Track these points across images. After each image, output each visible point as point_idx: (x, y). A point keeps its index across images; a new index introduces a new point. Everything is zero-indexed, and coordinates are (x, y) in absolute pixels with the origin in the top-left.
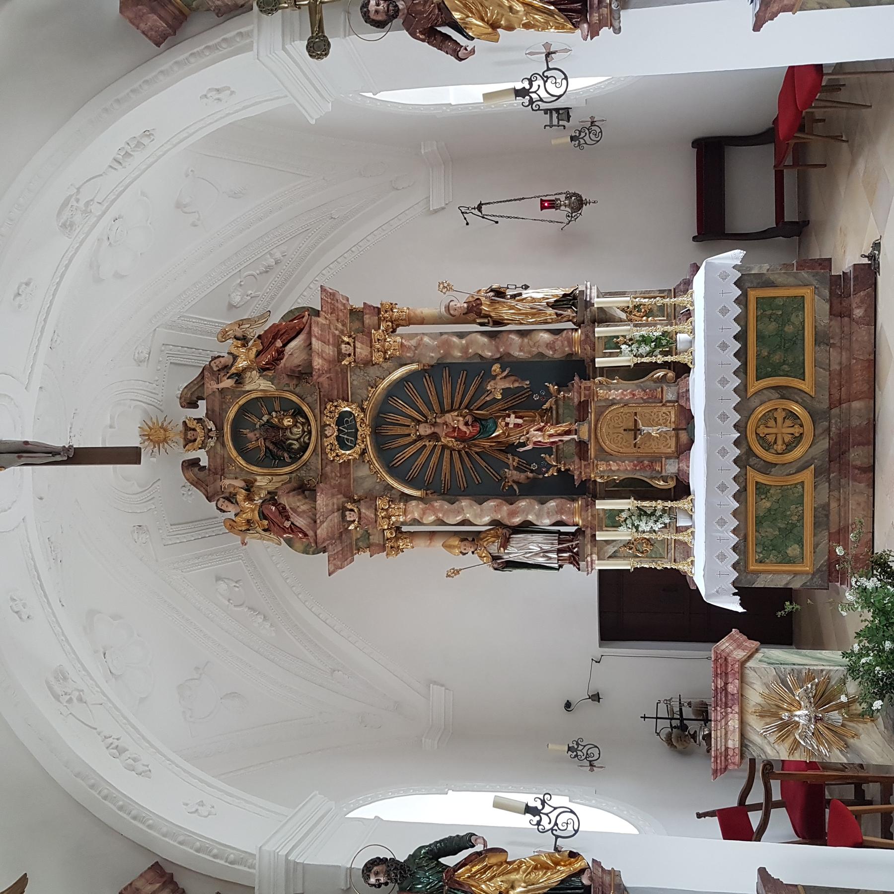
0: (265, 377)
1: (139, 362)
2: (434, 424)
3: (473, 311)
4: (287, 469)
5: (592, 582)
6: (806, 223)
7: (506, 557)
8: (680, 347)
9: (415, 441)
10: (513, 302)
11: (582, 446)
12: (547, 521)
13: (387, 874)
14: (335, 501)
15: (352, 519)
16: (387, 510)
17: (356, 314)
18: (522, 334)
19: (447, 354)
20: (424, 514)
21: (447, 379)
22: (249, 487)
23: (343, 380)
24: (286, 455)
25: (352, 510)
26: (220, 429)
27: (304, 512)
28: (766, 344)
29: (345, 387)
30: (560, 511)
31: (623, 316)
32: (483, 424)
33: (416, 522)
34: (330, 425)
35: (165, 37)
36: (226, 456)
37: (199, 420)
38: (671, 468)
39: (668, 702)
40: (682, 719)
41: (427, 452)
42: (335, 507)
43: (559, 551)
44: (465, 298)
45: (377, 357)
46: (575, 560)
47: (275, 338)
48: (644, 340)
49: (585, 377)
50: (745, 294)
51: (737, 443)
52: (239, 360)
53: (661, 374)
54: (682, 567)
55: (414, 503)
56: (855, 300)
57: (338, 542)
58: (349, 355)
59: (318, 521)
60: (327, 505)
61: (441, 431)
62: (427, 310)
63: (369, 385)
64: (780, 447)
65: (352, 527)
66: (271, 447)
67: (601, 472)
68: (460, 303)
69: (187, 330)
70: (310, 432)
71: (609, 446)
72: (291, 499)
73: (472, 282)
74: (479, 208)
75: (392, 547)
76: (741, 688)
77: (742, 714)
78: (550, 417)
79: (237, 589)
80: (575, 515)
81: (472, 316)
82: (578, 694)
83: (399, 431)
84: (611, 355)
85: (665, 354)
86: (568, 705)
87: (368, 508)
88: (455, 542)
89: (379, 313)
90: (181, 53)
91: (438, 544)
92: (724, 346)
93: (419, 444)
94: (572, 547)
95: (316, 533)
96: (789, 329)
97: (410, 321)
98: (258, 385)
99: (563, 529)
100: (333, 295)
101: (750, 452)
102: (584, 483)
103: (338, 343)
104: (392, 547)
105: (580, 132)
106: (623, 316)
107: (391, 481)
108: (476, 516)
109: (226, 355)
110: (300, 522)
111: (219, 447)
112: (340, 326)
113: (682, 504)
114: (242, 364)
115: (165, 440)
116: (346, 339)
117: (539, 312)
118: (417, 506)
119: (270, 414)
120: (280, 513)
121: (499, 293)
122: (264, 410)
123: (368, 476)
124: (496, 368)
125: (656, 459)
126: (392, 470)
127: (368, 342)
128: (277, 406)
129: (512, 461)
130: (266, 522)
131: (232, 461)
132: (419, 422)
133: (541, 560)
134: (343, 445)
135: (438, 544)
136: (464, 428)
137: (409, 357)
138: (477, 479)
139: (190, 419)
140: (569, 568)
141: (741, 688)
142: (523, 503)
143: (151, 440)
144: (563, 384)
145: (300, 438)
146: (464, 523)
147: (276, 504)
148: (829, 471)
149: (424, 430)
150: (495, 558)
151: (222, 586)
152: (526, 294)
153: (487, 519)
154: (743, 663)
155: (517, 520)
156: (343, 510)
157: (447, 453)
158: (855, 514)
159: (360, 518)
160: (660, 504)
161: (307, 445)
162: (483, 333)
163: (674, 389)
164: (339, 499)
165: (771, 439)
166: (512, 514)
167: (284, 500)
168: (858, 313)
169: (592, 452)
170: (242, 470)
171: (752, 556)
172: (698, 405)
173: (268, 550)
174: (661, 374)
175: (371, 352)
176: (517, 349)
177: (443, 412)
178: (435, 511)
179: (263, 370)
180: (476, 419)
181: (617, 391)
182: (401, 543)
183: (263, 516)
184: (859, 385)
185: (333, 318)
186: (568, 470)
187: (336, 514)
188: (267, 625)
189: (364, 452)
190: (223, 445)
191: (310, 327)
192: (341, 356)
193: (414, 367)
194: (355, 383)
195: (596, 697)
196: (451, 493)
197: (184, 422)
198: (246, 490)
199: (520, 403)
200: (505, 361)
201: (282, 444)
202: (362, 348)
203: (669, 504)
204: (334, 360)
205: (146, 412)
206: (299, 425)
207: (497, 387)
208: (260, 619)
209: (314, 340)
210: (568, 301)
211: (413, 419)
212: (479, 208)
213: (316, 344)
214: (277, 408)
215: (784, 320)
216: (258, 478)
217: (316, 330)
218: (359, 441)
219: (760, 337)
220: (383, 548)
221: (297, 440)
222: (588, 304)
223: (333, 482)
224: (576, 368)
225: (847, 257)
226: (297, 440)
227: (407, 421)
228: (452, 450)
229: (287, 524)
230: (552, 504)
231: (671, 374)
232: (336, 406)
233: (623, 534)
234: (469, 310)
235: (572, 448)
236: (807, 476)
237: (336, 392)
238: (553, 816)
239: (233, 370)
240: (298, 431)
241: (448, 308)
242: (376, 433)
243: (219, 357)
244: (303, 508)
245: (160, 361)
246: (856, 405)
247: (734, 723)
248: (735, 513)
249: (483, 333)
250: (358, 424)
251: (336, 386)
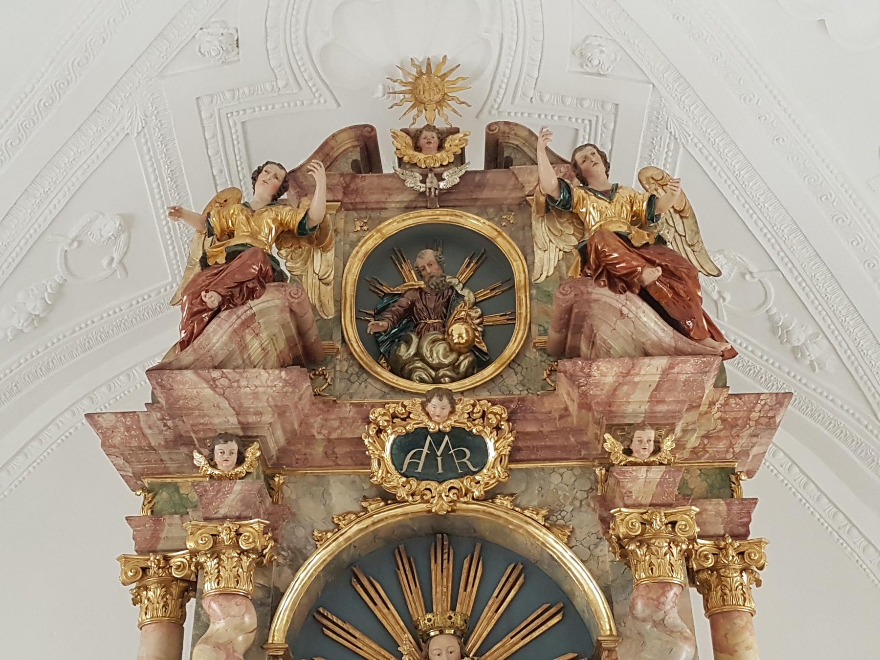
1: (582, 55)
4: (352, 334)
9: (412, 627)
14: (268, 418)
15: (218, 458)
16: (236, 546)
17: (724, 482)
20: (217, 646)
23: (564, 448)
24: (384, 324)
25: (240, 460)
26: (444, 199)
27: (244, 347)
29: (543, 454)
33: (203, 624)
34: (453, 412)
36: (384, 214)
37: (460, 159)
42: (252, 419)
52: (604, 204)
55: (250, 620)
57: (169, 434)
58: (628, 452)
59: (216, 374)
60: (256, 395)
63: (551, 512)
65: (199, 459)
66: (404, 302)
72: (276, 316)
75: (144, 569)
79: (105, 262)
83: (440, 590)
87: (245, 502)
89: (735, 537)
95: (186, 368)
97: (720, 618)
100: (771, 425)
103: (663, 425)
104: (144, 569)
107: (316, 560)
109: (612, 181)
111: (406, 198)
112: (693, 441)
114: (593, 211)
115: (419, 103)
116: (668, 444)
118: (240, 629)
119: (476, 304)
120: (241, 284)
122: (484, 294)
123: (329, 510)
126: (343, 573)
127: (664, 499)
130: (221, 260)
131: (374, 224)
132: (463, 636)
134: (409, 443)
137: (632, 607)
139: (464, 140)
143: (417, 78)
145: (423, 360)
151: (110, 226)
159: (220, 478)
167: (269, 302)
170: (353, 245)
175: (640, 506)
182: (154, 593)
185: (713, 423)
187: (233, 420)
189: (388, 498)
190: (409, 208)
191: (693, 354)
192: (625, 432)
193: (606, 625)
194: (556, 479)
197: (457, 131)
198: (302, 224)
201: (409, 321)
202: (647, 482)
204: (610, 414)
206: (453, 356)
209: (662, 362)
211: (471, 623)
213: (652, 369)
214: (489, 320)
216: (330, 255)
217: (687, 367)
218: (414, 482)
221: (418, 354)
223: (316, 422)
226: (418, 354)
227: (465, 605)
229: (212, 299)
232: (498, 428)
237: (531, 428)
239: (578, 193)
240: (438, 354)
243: (607, 166)
244: (254, 347)
245: (580, 101)
250: (455, 483)
251: (546, 429)
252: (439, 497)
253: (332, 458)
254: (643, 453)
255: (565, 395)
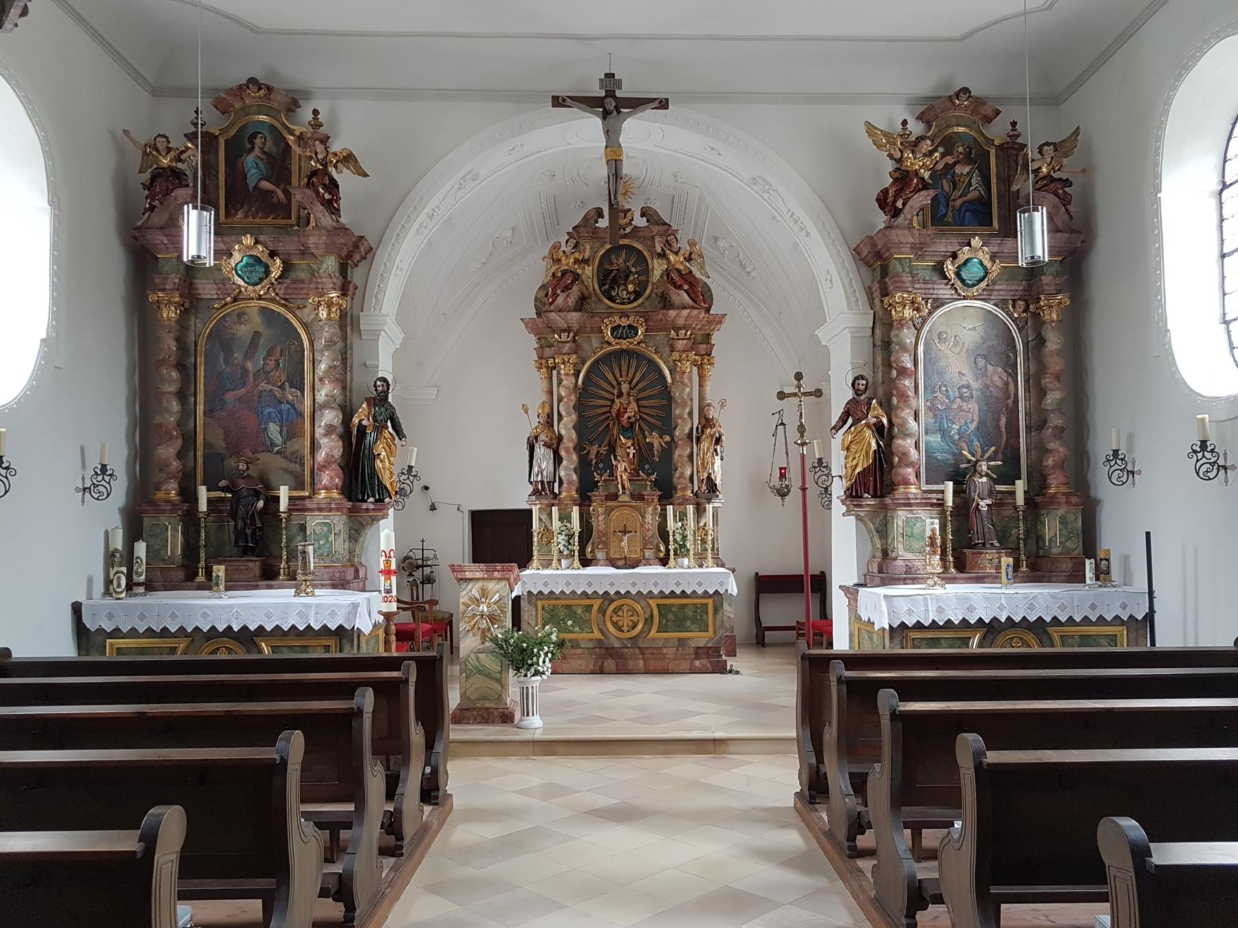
0: (661, 276)
2: (629, 395)
3: (707, 422)
5: (523, 505)
6: (764, 645)
7: (537, 446)
8: (679, 560)
10: (712, 450)
11: (615, 497)
12: (562, 474)
13: (383, 391)
18: (691, 456)
19: (678, 405)
21: (660, 404)
22: (585, 261)
28: (679, 611)
30: (569, 483)
31: (702, 524)
32: (628, 430)
35: (859, 254)
38: (600, 555)
39: (435, 557)
40: (423, 566)
41: (611, 389)
43: (542, 482)
44: (716, 416)
45: (676, 355)
46: (536, 492)
47: (690, 283)
48: (684, 538)
49: (660, 498)
50: (710, 596)
51: (618, 593)
53: (662, 549)
54: (535, 563)
55: (574, 381)
56: (705, 662)
61: (624, 400)
62: (708, 389)
64: (615, 619)
67: (598, 509)
68: (712, 414)
69: (696, 224)
70: (623, 303)
71: (615, 514)
73: (727, 422)
74: (782, 424)
76: (496, 579)
77: (483, 579)
78: (634, 476)
80: (569, 492)
81: (703, 422)
82: (435, 495)
83: (624, 368)
84: (675, 516)
85: (675, 551)
86: (426, 488)
88: (547, 411)
90: (849, 263)
91: (544, 397)
92: (678, 584)
93: (614, 383)
94: (543, 490)
96: (688, 623)
97: (702, 377)
98: (658, 268)
99: (556, 485)
101: (612, 601)
102: (589, 498)
103: (686, 328)
105: (1122, 459)
106: (702, 524)
107: (588, 364)
108: (565, 425)
110: (560, 300)
113: (577, 563)
114: (672, 257)
117: (704, 468)
121: (718, 441)
122: (639, 268)
124: (668, 438)
125: (606, 545)
126: (596, 362)
128: (641, 278)
129: (603, 450)
133: (535, 469)
134: (613, 329)
135: (544, 397)
136: (626, 416)
138: (590, 424)
140: (531, 489)
141: (496, 579)
142: (575, 457)
144: (656, 484)
146: (559, 414)
147: (573, 282)
148: (600, 648)
149: (625, 388)
150: (536, 438)
151: (509, 233)
152: (717, 459)
153: (563, 432)
154: (508, 579)
155: (563, 453)
156: (568, 330)
157: (609, 403)
158: (575, 664)
160: (576, 548)
161: (614, 301)
162: (692, 429)
163: (652, 556)
164: (575, 327)
165: (620, 613)
166: (567, 450)
168: (697, 663)
169: (610, 503)
171: (546, 603)
172: (641, 570)
173: (537, 272)
174: (662, 549)
176: (680, 453)
177: (637, 401)
178: (568, 396)
179: (667, 273)
180: (632, 424)
181: (651, 520)
183: (564, 273)
184: (652, 665)
186: (597, 487)
188: (479, 266)
192: (677, 329)
193: (669, 380)
195: (433, 508)
196: (580, 407)
199: (644, 453)
200: (672, 445)
201: (615, 283)
203: (577, 554)
205: (638, 178)
207: (655, 439)
208: (484, 260)
210: (712, 487)
212: (782, 424)
213: (685, 312)
215: (694, 620)
217: (695, 312)
219: (683, 606)
220: (540, 358)
222: (709, 501)
224: (667, 492)
225: (731, 662)
227: (631, 374)
228: (611, 407)
230: (575, 477)
231: (662, 555)
233: (556, 524)
234: (707, 420)
235: (612, 490)
236: (597, 634)
238: (103, 483)
239: (668, 252)
241: (709, 405)
242: (622, 351)
246: (641, 663)
247: (478, 575)
248: (573, 592)
249: (692, 429)
252: (624, 344)
253: (592, 331)
254: (682, 336)
255: (661, 316)
